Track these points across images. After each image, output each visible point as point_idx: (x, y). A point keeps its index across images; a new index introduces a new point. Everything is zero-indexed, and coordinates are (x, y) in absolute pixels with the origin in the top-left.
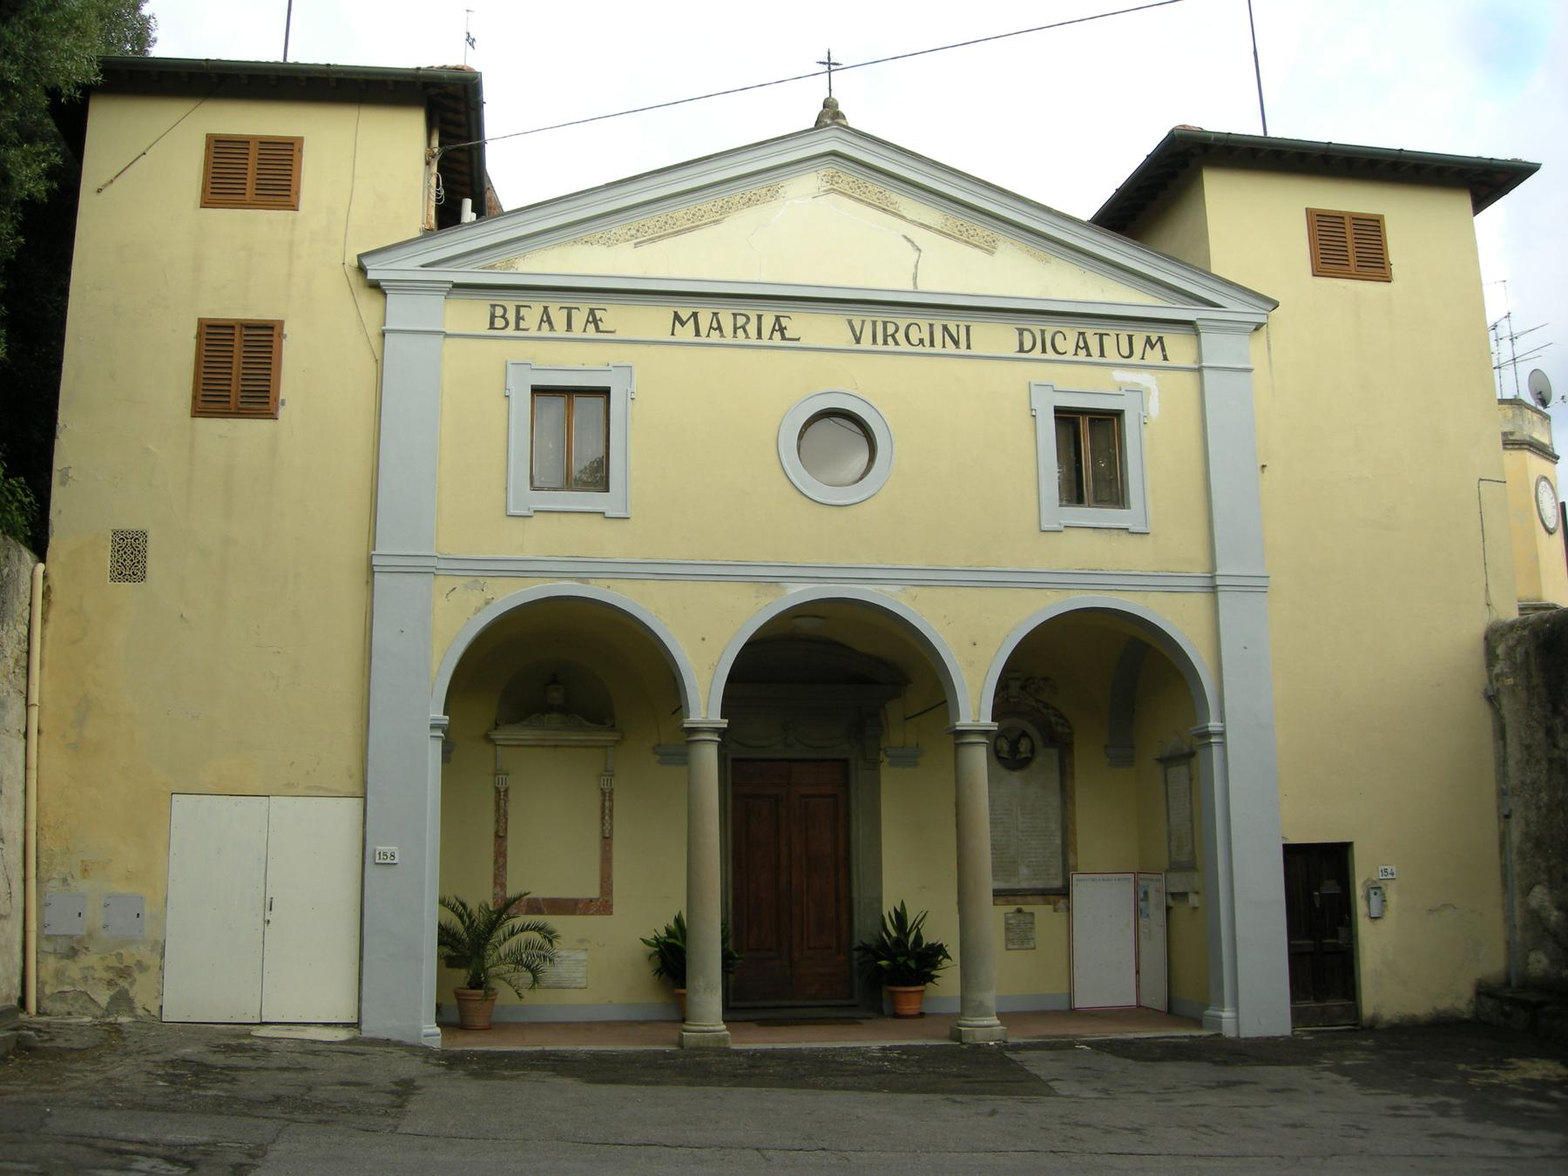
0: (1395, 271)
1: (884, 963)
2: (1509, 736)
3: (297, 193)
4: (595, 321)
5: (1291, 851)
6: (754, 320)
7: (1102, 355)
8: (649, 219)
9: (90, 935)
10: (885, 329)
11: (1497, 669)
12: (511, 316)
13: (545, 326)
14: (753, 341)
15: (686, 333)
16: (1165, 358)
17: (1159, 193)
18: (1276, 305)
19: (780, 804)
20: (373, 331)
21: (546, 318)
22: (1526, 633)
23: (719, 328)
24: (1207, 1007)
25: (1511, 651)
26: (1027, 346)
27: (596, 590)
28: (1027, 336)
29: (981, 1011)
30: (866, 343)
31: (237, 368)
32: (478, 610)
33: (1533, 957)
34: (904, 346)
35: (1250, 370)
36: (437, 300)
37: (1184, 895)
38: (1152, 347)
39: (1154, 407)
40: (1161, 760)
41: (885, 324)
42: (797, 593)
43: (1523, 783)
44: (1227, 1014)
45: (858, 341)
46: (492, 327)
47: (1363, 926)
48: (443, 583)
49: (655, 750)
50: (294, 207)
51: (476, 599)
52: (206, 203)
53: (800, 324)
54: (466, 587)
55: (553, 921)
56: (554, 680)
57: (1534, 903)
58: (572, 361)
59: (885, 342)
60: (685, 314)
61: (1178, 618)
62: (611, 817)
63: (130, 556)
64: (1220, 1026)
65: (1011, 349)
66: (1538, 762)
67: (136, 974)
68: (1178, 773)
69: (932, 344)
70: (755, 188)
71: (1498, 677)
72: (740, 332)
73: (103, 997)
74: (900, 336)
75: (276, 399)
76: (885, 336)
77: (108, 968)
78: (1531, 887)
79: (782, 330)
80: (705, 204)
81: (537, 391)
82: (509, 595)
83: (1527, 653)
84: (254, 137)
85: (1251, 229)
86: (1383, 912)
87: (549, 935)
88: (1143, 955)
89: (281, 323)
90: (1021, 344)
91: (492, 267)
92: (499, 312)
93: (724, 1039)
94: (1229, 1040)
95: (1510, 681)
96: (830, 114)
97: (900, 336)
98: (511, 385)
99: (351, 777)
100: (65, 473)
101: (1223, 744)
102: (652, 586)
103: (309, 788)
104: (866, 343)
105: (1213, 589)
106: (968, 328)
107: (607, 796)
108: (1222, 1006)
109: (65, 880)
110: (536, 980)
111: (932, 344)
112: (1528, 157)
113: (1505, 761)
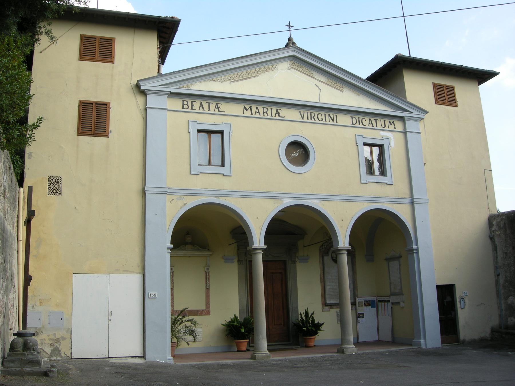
0: (458, 104)
1: (305, 329)
2: (498, 250)
3: (114, 57)
4: (218, 108)
5: (439, 287)
6: (270, 110)
7: (377, 126)
8: (234, 74)
9: (43, 327)
10: (311, 115)
11: (493, 229)
12: (190, 104)
13: (201, 108)
14: (270, 117)
15: (248, 113)
16: (395, 128)
17: (391, 74)
18: (427, 112)
19: (275, 276)
20: (142, 107)
21: (202, 106)
22: (504, 217)
23: (259, 112)
24: (413, 339)
25: (498, 224)
26: (354, 122)
27: (221, 201)
28: (354, 119)
29: (349, 343)
30: (305, 119)
31: (93, 119)
32: (181, 207)
33: (509, 319)
34: (317, 121)
35: (420, 133)
36: (165, 98)
37: (398, 303)
38: (247, 110)
39: (392, 144)
40: (386, 259)
41: (311, 113)
42: (287, 203)
43: (504, 264)
44: (422, 341)
45: (303, 118)
46: (183, 108)
47: (460, 312)
48: (168, 197)
49: (223, 257)
50: (113, 62)
51: (181, 203)
52: (81, 58)
53: (285, 112)
54: (177, 199)
55: (196, 318)
56: (188, 234)
57: (509, 302)
58: (211, 121)
59: (311, 119)
60: (247, 107)
61: (402, 212)
62: (209, 281)
63: (55, 186)
64: (421, 345)
65: (350, 124)
66: (510, 258)
67: (61, 341)
68: (394, 264)
69: (326, 121)
70: (269, 66)
71: (493, 231)
72: (265, 114)
73: (49, 350)
74: (316, 117)
75: (108, 130)
76: (311, 117)
77: (50, 339)
78: (508, 297)
79: (279, 114)
80: (253, 70)
81: (200, 131)
82: (192, 202)
83: (505, 224)
84: (98, 37)
85: (418, 89)
86: (464, 306)
87: (194, 323)
88: (380, 324)
89: (109, 103)
90: (353, 122)
91: (183, 87)
92: (185, 103)
93: (268, 356)
94: (424, 349)
95: (499, 233)
96: (290, 43)
97: (316, 117)
98: (190, 128)
99: (138, 267)
100: (30, 154)
101: (418, 253)
102: (240, 199)
103: (124, 271)
104: (305, 119)
105: (412, 203)
106: (336, 116)
107: (207, 274)
108: (420, 338)
109: (33, 307)
110: (195, 339)
111: (326, 121)
112: (496, 70)
113: (497, 258)
